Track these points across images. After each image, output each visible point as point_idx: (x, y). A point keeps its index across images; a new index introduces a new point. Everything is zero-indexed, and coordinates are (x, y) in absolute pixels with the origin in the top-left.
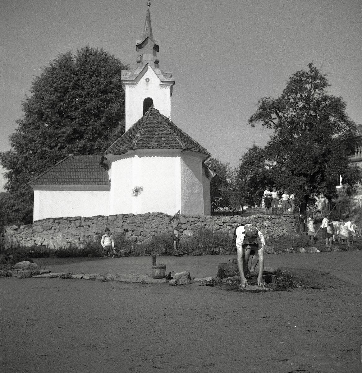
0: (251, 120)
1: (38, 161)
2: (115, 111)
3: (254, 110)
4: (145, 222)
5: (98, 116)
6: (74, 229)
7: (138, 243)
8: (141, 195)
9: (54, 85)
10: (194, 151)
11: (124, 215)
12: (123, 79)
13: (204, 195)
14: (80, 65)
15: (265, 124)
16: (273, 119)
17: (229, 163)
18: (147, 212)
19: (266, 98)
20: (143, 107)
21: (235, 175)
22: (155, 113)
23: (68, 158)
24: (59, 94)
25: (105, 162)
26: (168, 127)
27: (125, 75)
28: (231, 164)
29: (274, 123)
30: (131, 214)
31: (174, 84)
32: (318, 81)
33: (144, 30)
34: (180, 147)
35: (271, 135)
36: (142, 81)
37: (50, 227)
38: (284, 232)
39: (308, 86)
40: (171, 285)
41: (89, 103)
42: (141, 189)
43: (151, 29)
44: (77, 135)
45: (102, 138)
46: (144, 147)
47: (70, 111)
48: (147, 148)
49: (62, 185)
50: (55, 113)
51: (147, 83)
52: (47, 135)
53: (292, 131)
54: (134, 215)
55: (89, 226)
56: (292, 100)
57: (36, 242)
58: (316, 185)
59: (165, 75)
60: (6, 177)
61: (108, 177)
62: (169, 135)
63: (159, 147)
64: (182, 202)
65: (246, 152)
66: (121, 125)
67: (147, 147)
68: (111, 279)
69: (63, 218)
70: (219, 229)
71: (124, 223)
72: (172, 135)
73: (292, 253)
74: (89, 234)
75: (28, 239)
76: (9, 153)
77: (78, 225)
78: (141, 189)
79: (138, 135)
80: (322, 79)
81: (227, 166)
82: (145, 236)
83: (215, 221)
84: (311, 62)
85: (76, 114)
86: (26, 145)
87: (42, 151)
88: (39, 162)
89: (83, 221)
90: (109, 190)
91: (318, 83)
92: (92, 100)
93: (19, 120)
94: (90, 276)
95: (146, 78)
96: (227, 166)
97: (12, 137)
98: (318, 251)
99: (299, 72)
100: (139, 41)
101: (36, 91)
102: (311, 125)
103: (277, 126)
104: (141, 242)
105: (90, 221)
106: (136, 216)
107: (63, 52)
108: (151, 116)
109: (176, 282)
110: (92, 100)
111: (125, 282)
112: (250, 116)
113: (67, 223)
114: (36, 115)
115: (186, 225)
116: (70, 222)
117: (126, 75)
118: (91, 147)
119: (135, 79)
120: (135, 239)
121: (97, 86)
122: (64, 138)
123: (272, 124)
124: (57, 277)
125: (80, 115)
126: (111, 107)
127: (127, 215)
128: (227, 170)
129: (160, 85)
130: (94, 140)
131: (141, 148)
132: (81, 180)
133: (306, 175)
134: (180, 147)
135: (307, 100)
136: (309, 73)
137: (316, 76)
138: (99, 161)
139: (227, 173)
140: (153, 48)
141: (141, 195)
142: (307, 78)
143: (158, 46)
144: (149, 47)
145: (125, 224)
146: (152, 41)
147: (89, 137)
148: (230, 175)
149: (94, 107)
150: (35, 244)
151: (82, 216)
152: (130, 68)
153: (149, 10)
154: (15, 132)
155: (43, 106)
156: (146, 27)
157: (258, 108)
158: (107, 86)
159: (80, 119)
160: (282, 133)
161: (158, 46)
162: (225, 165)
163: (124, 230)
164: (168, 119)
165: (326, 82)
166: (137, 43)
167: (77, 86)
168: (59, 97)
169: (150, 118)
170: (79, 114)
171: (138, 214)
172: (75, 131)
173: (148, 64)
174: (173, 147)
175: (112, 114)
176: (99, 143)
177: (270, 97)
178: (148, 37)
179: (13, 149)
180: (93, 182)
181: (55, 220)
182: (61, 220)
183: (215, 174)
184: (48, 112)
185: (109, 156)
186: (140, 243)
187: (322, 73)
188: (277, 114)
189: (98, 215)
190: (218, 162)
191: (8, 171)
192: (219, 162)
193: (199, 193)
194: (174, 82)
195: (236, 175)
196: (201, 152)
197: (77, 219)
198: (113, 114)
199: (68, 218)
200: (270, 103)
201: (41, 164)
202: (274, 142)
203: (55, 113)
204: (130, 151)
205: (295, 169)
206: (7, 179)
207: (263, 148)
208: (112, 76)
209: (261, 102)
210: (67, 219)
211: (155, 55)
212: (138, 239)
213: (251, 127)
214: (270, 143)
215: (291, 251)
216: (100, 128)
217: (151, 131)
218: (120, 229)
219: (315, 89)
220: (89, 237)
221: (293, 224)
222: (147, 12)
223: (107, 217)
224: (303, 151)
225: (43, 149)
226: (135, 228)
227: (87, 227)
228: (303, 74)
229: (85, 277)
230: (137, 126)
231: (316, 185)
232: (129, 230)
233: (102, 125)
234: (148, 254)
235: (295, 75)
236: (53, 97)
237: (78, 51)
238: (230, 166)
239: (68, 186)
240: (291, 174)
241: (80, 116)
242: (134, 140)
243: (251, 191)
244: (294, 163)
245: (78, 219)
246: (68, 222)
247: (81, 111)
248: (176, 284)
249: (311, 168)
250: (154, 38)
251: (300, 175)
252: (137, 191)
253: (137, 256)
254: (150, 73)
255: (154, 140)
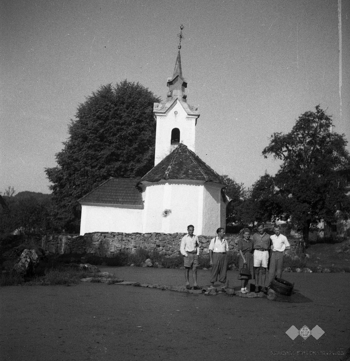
0: (264, 152)
1: (81, 178)
2: (147, 138)
3: (267, 143)
4: (173, 240)
5: (131, 142)
6: (117, 242)
7: (167, 257)
8: (169, 216)
9: (97, 114)
10: (215, 182)
11: (157, 234)
12: (156, 110)
13: (221, 218)
14: (119, 96)
15: (276, 155)
16: (284, 151)
17: (243, 184)
18: (176, 232)
19: (278, 133)
20: (171, 136)
21: (248, 195)
22: (184, 148)
23: (109, 180)
24: (101, 122)
25: (140, 185)
26: (194, 161)
27: (157, 108)
28: (245, 184)
29: (284, 155)
30: (163, 233)
31: (199, 117)
32: (324, 121)
33: (175, 69)
34: (203, 179)
35: (281, 164)
36: (171, 113)
37: (98, 239)
38: (286, 253)
39: (315, 125)
40: (206, 295)
41: (125, 130)
42: (170, 211)
43: (180, 68)
44: (113, 157)
45: (135, 160)
46: (174, 178)
47: (109, 136)
48: (177, 179)
49: (105, 203)
50: (97, 137)
51: (175, 115)
52: (90, 156)
53: (300, 163)
54: (165, 234)
55: (129, 241)
56: (300, 136)
57: (86, 250)
58: (317, 211)
59: (191, 108)
60: (51, 189)
61: (142, 198)
62: (195, 168)
63: (186, 178)
64: (203, 223)
65: (259, 179)
66: (152, 150)
67: (177, 178)
68: (167, 288)
69: (108, 232)
70: (232, 249)
71: (156, 240)
72: (197, 168)
73: (289, 272)
74: (129, 247)
75: (79, 247)
76: (55, 168)
77: (120, 239)
78: (170, 211)
79: (170, 167)
80: (327, 119)
81: (241, 186)
82: (173, 252)
83: (230, 242)
84: (318, 105)
85: (114, 139)
86: (72, 163)
87: (85, 170)
88: (81, 179)
89: (124, 236)
90: (142, 208)
91: (323, 122)
92: (127, 127)
93: (66, 142)
94: (153, 286)
95: (174, 111)
96: (241, 186)
97: (59, 155)
98: (311, 271)
99: (306, 113)
100: (171, 79)
101: (81, 118)
102: (316, 159)
103: (286, 158)
104: (169, 256)
105: (130, 236)
106: (166, 234)
107: (105, 84)
108: (180, 151)
109: (209, 293)
110: (127, 127)
111: (176, 291)
112: (264, 149)
113: (112, 237)
114: (81, 139)
115: (206, 244)
116: (114, 236)
117: (157, 107)
118: (125, 168)
119: (165, 112)
120: (165, 253)
121: (133, 116)
122: (103, 160)
123: (282, 155)
124: (130, 285)
125: (117, 140)
126: (144, 134)
127: (160, 233)
128: (241, 190)
129: (187, 117)
130: (128, 161)
131: (171, 178)
132: (120, 200)
133: (309, 203)
134: (203, 179)
135: (314, 136)
136: (316, 114)
137: (321, 116)
138: (136, 184)
139: (242, 192)
140: (182, 85)
141: (169, 216)
142: (314, 118)
143: (186, 84)
144: (179, 84)
145: (158, 241)
146: (181, 78)
147: (123, 159)
148: (244, 195)
149: (129, 134)
150: (85, 252)
151: (124, 232)
152: (161, 100)
153: (179, 52)
154: (61, 151)
155: (87, 131)
156: (177, 67)
157: (271, 142)
158: (140, 116)
159: (117, 144)
160: (290, 164)
161: (186, 84)
162: (240, 185)
163: (157, 245)
164: (194, 153)
165: (331, 122)
166: (169, 80)
167: (116, 115)
168: (100, 124)
169: (180, 152)
170: (117, 140)
171: (168, 234)
172: (113, 154)
173: (177, 99)
174: (198, 179)
175: (144, 140)
176: (132, 165)
177: (281, 133)
178: (178, 76)
179: (60, 167)
180: (129, 202)
181: (102, 234)
182: (106, 235)
183: (231, 200)
184: (91, 137)
185: (144, 182)
186: (169, 257)
187: (327, 113)
188: (287, 147)
189: (137, 232)
190: (234, 182)
191: (53, 184)
192: (235, 183)
193: (217, 217)
194: (199, 116)
195: (249, 195)
196: (220, 183)
197: (119, 234)
198: (145, 140)
199: (112, 233)
200: (282, 138)
201: (83, 181)
202: (283, 170)
203: (97, 137)
204: (162, 180)
205: (300, 197)
206: (52, 191)
207: (274, 176)
208: (146, 107)
209: (274, 136)
210: (112, 233)
211: (183, 91)
212: (167, 253)
213: (264, 158)
214: (281, 172)
215: (289, 270)
216: (134, 152)
217: (180, 164)
218: (153, 245)
219: (320, 128)
220: (129, 249)
221: (294, 247)
222: (178, 53)
223: (144, 234)
224: (307, 181)
225: (86, 168)
226: (165, 244)
227: (127, 241)
228: (311, 114)
229: (150, 286)
230: (168, 159)
231: (317, 211)
232: (160, 245)
233: (135, 149)
234: (176, 266)
235: (303, 115)
236: (96, 124)
237: (117, 85)
238: (244, 186)
239: (109, 204)
240: (296, 200)
241: (118, 141)
242: (166, 171)
243: (261, 213)
244: (299, 191)
245: (120, 235)
246: (112, 236)
247: (119, 137)
248: (209, 295)
249: (314, 197)
250: (183, 76)
251: (304, 202)
252: (166, 213)
253: (168, 268)
254: (179, 107)
255: (183, 172)
